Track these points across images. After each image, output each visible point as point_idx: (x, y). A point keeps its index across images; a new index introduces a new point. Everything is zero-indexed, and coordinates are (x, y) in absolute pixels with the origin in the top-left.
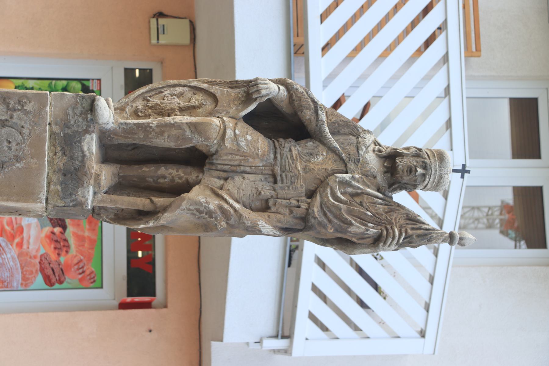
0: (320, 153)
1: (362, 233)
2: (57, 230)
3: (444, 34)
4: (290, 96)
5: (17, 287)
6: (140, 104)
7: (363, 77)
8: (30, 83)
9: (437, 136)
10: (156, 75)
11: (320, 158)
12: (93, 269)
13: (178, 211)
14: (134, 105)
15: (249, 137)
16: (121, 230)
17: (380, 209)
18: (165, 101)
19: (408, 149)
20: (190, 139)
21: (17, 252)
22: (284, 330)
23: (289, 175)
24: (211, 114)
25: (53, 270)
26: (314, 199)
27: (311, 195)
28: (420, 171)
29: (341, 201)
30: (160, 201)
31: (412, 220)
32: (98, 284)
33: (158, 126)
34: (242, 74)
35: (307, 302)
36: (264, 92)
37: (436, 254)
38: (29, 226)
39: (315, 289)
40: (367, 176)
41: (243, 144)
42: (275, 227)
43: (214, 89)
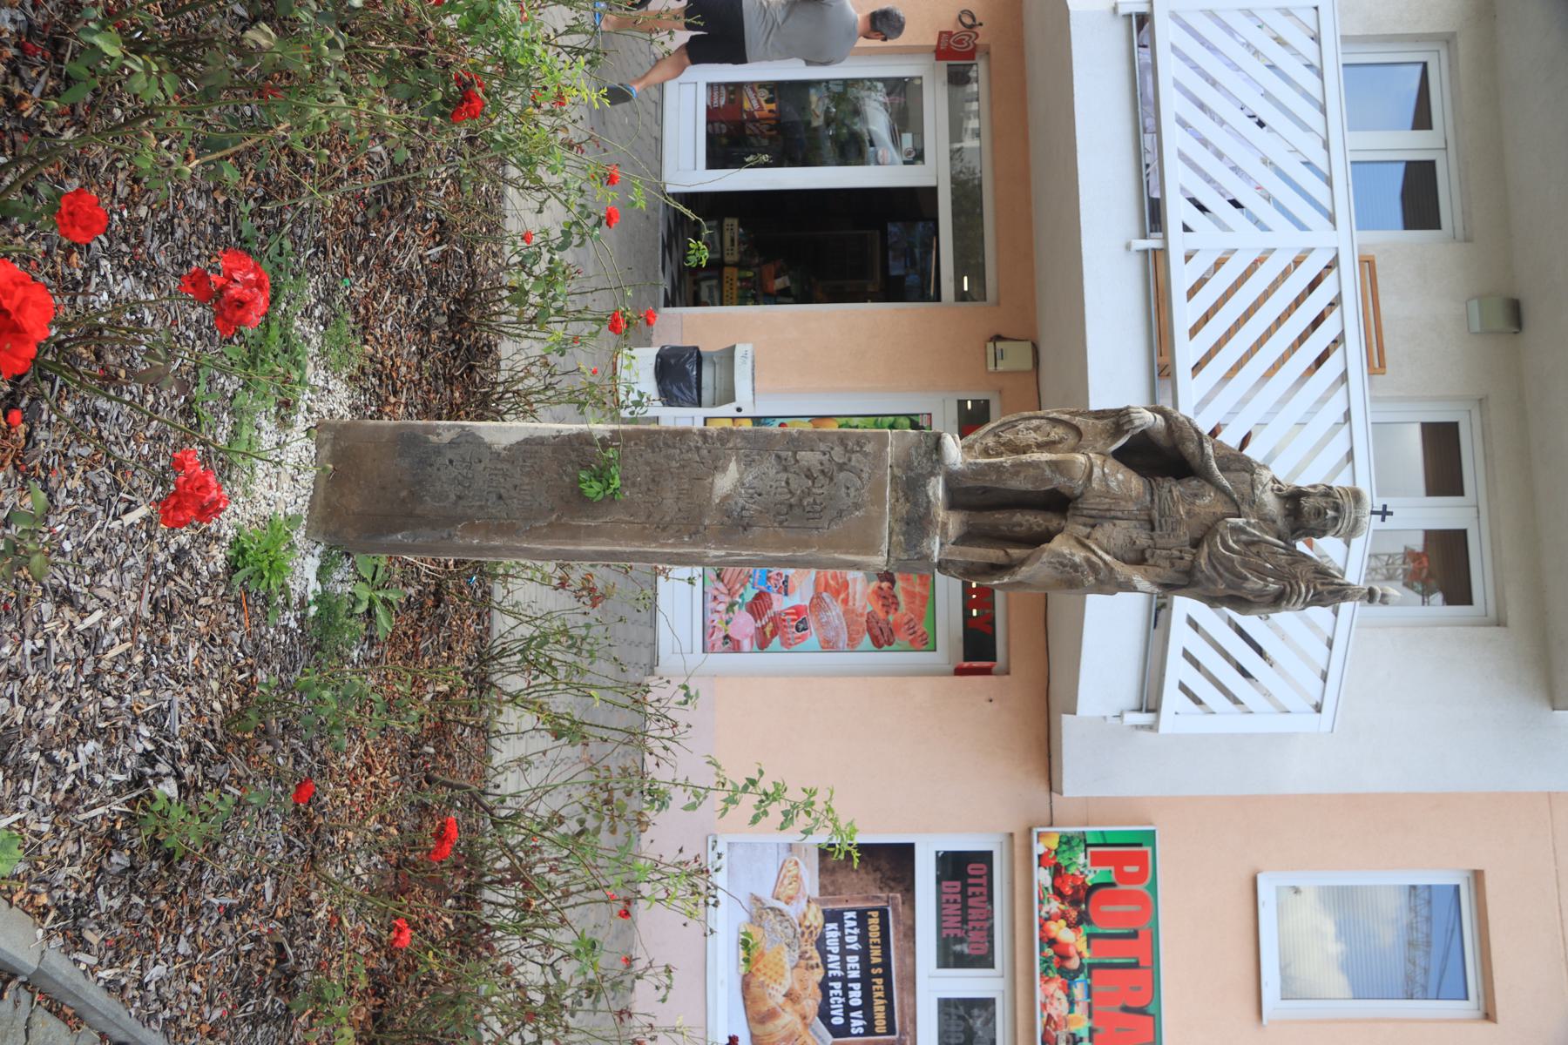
1: (1261, 590)
2: (885, 585)
3: (1340, 349)
6: (990, 441)
7: (1244, 401)
8: (855, 421)
9: (1336, 471)
10: (994, 409)
11: (1207, 500)
13: (1038, 565)
15: (1120, 477)
16: (957, 585)
19: (1314, 487)
20: (1051, 480)
22: (1150, 703)
23: (1170, 520)
24: (1074, 450)
27: (1196, 544)
28: (1331, 513)
30: (1016, 553)
31: (1322, 573)
32: (931, 646)
33: (1013, 465)
34: (1100, 400)
35: (1176, 669)
36: (1137, 423)
37: (1336, 613)
38: (855, 580)
39: (1187, 655)
40: (1264, 520)
41: (1113, 484)
42: (1153, 583)
43: (1077, 420)
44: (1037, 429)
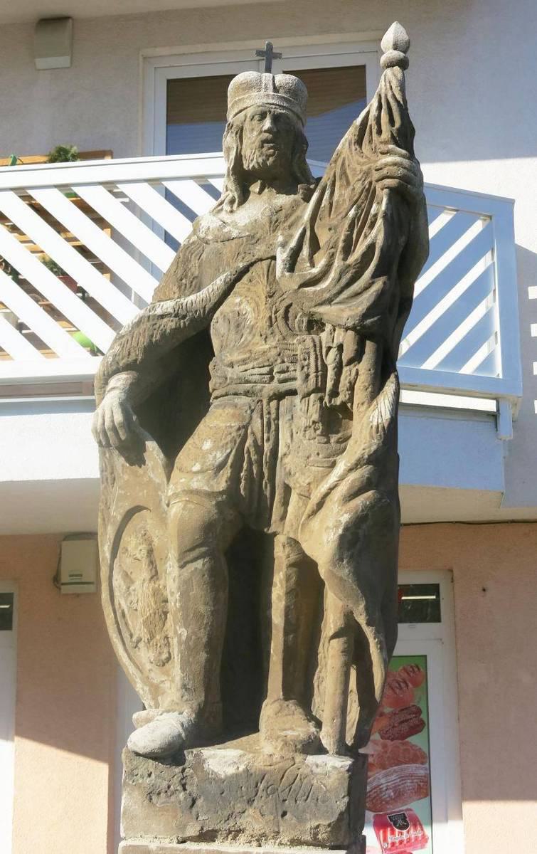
0: (237, 309)
4: (127, 368)
5: (426, 769)
11: (247, 308)
12: (401, 668)
14: (148, 666)
17: (341, 195)
18: (139, 609)
21: (378, 770)
25: (402, 722)
26: (325, 318)
29: (329, 266)
44: (127, 576)
